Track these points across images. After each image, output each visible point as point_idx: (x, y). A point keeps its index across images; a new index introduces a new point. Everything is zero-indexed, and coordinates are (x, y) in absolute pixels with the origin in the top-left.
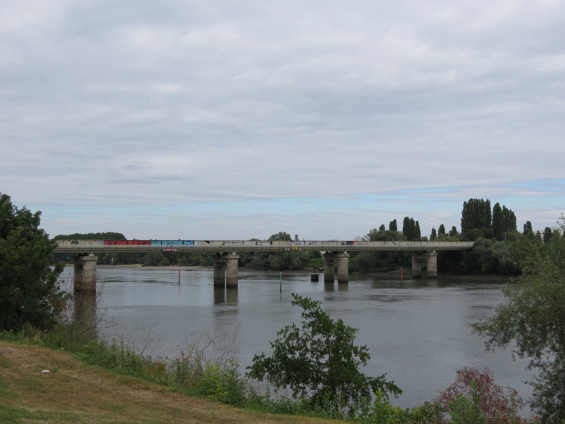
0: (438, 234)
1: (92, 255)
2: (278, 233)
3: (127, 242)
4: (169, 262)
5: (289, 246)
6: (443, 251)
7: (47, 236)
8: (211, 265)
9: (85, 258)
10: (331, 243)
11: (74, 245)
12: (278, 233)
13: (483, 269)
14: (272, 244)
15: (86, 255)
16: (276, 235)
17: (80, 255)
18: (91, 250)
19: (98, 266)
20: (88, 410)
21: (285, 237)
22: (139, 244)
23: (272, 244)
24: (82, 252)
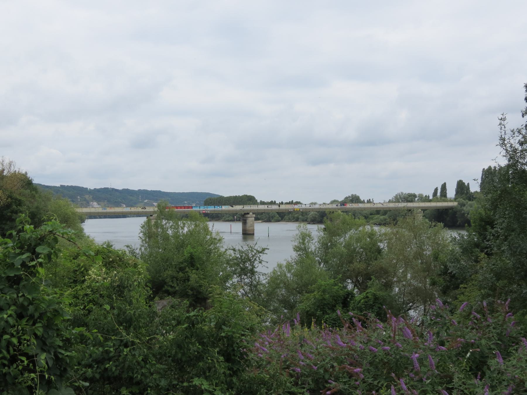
0: (127, 206)
1: (251, 214)
2: (350, 195)
3: (363, 202)
4: (280, 218)
5: (293, 208)
6: (439, 209)
7: (476, 192)
8: (239, 220)
9: (248, 216)
10: (314, 205)
11: (143, 210)
12: (350, 195)
13: (458, 223)
14: (279, 206)
15: (248, 214)
16: (349, 197)
17: (245, 214)
18: (251, 210)
19: (255, 222)
20: (42, 253)
21: (355, 199)
22: (185, 208)
23: (279, 206)
24: (246, 212)
